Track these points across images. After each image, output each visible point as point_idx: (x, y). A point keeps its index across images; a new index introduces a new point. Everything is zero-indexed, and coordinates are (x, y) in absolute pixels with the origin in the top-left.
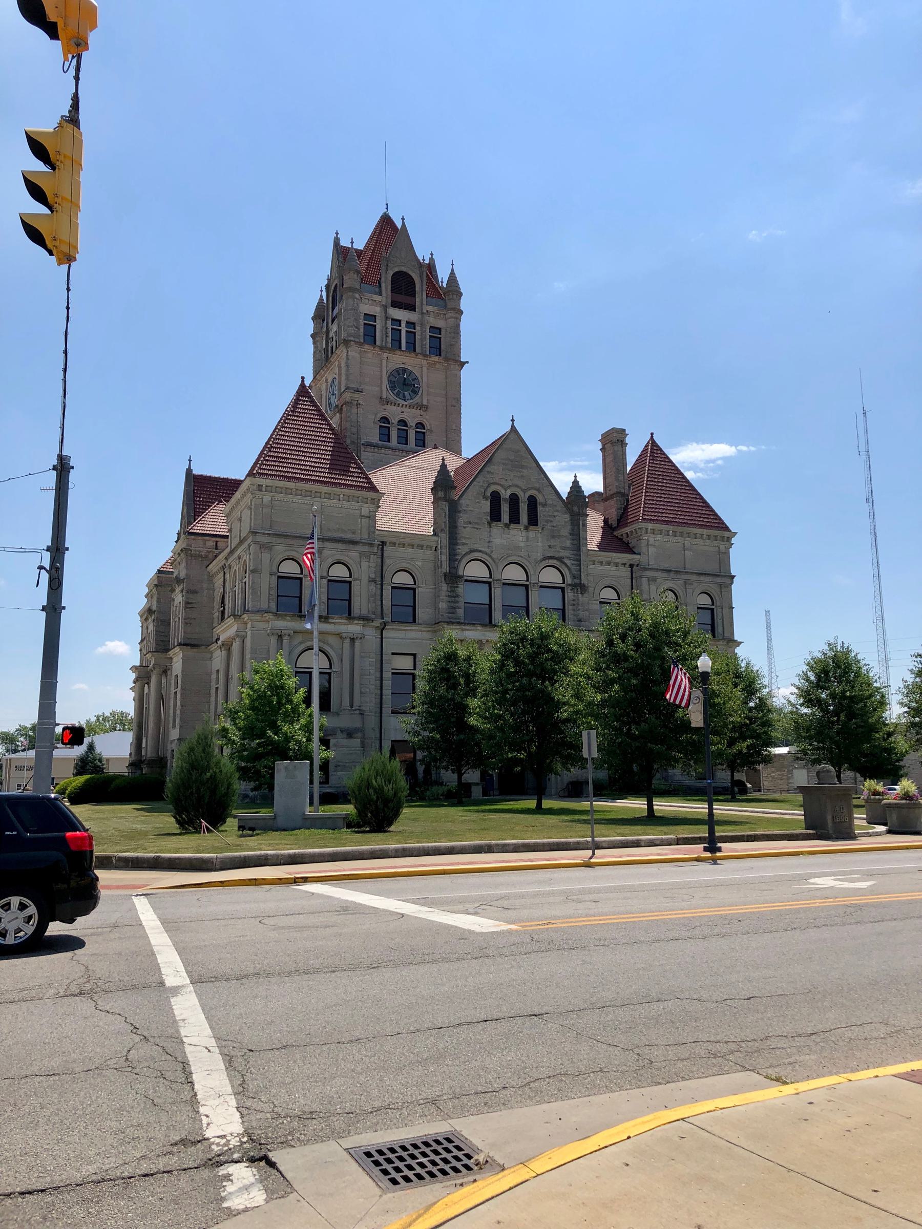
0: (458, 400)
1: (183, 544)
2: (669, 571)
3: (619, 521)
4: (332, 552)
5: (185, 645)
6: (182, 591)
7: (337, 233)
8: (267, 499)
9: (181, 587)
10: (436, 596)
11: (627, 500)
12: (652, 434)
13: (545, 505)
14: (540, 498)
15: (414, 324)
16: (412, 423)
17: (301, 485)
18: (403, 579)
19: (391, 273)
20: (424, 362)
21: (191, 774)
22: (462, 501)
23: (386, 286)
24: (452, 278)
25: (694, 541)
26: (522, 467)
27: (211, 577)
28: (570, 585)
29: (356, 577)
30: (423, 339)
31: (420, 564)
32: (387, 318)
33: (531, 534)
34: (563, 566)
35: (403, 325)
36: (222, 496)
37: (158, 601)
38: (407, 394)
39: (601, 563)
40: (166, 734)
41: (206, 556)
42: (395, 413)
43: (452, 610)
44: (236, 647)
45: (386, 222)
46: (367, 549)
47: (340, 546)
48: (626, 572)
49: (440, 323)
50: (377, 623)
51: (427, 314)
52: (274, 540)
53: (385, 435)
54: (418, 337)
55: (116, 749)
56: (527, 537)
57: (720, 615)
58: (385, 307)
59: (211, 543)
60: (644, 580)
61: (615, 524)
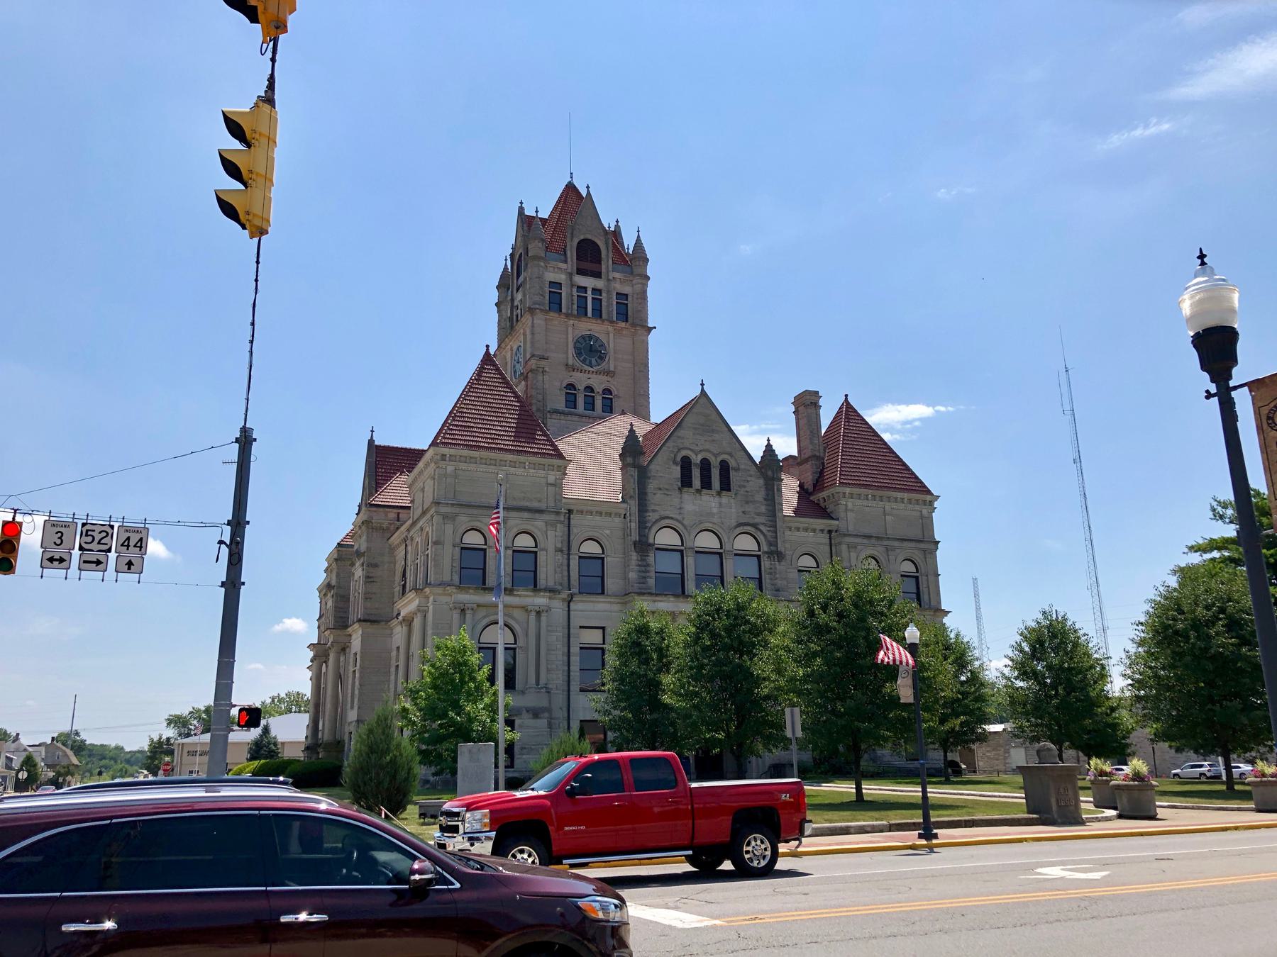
0: (647, 366)
1: (363, 516)
2: (869, 537)
3: (815, 486)
5: (365, 621)
8: (450, 469)
10: (626, 565)
13: (737, 470)
14: (732, 463)
17: (484, 454)
18: (591, 548)
19: (576, 241)
20: (611, 329)
22: (652, 467)
23: (572, 254)
25: (894, 505)
26: (713, 431)
27: (392, 550)
32: (572, 286)
33: (724, 500)
35: (589, 292)
37: (338, 575)
38: (593, 361)
39: (798, 529)
41: (388, 529)
42: (581, 380)
43: (643, 580)
44: (417, 622)
45: (570, 189)
46: (553, 517)
47: (526, 515)
48: (824, 538)
49: (626, 289)
50: (564, 595)
51: (614, 281)
52: (457, 510)
53: (571, 401)
58: (571, 275)
59: (392, 514)
60: (844, 547)
61: (811, 489)
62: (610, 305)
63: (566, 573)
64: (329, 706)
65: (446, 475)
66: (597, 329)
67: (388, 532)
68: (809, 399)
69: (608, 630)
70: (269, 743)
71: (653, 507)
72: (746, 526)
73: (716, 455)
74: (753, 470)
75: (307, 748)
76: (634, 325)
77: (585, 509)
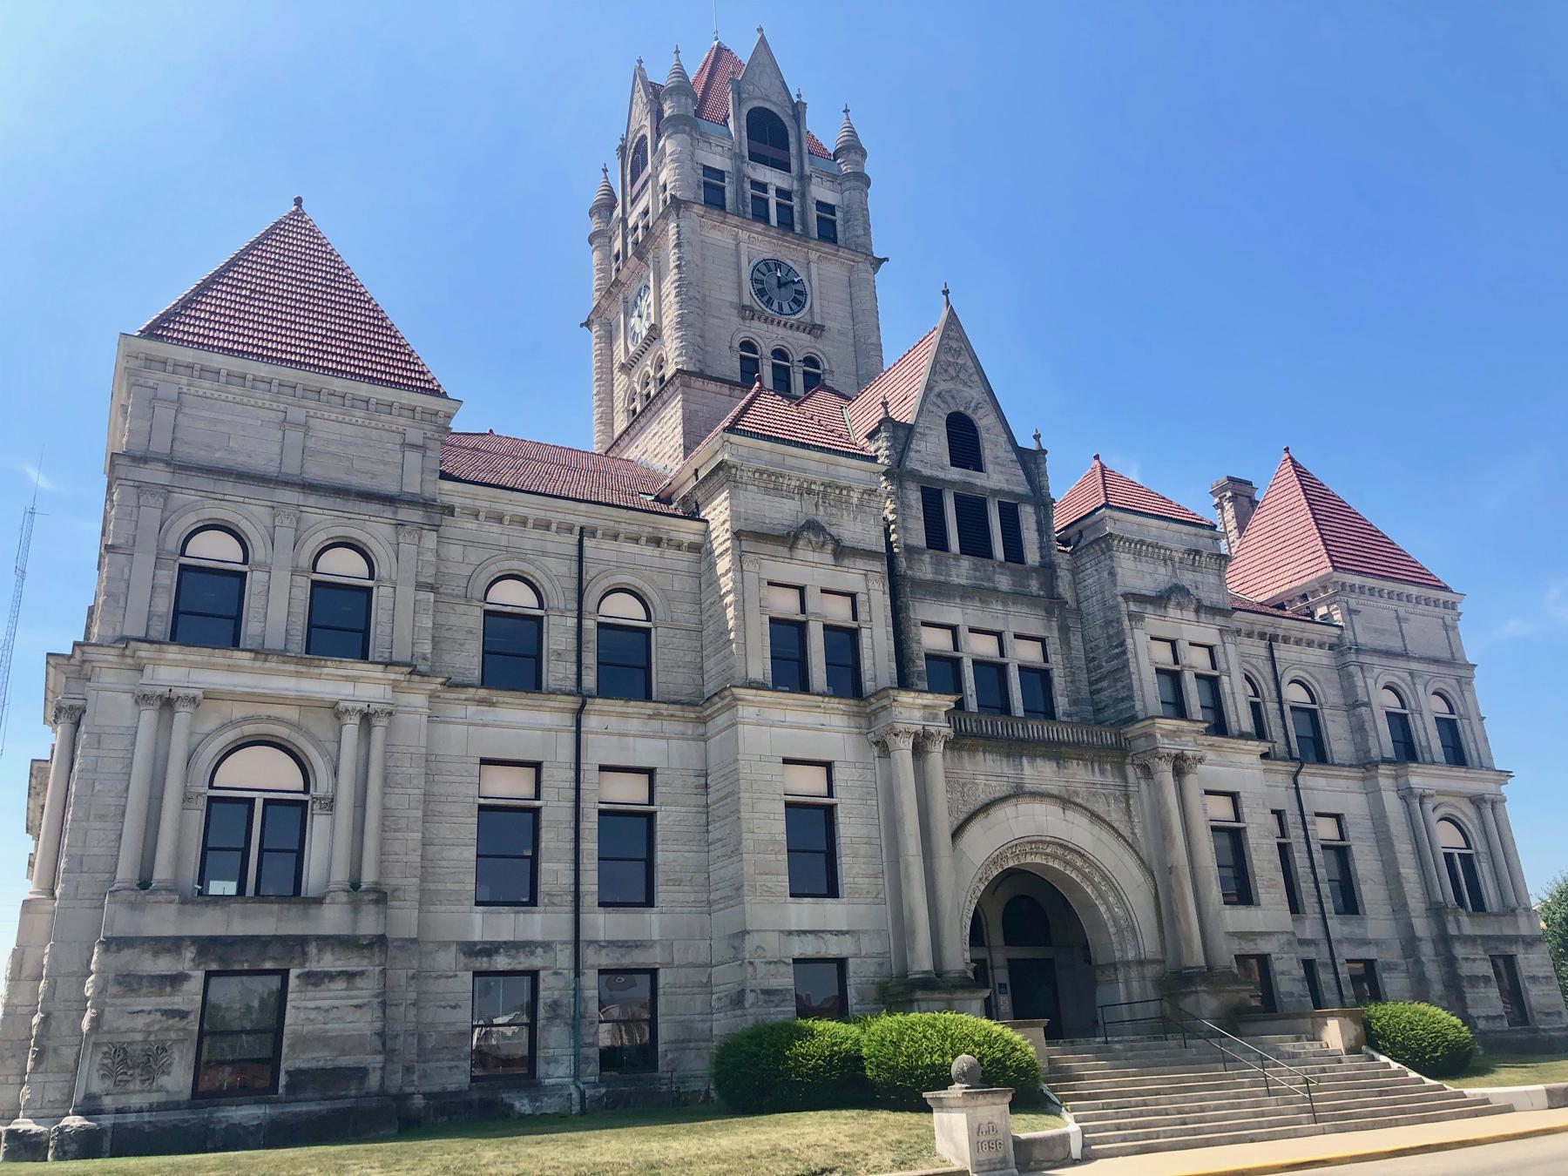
16: (797, 356)
18: (623, 609)
35: (772, 193)
42: (768, 337)
53: (749, 370)
57: (1419, 723)
66: (791, 254)
69: (658, 779)
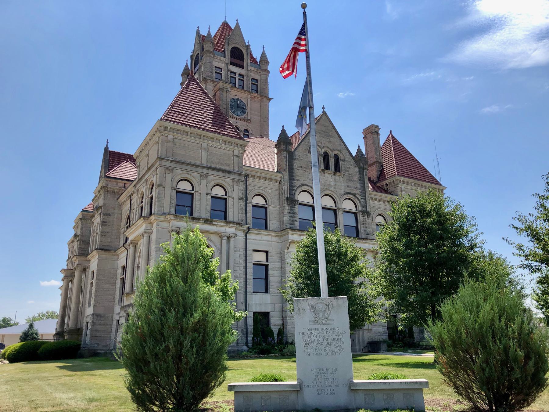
0: (268, 119)
1: (103, 184)
3: (379, 178)
4: (214, 177)
5: (100, 249)
6: (100, 214)
7: (198, 28)
8: (170, 137)
9: (100, 211)
10: (281, 213)
11: (382, 166)
12: (391, 131)
13: (344, 160)
14: (341, 156)
15: (257, 80)
17: (193, 130)
18: (259, 201)
19: (230, 47)
20: (249, 96)
21: (165, 315)
22: (296, 153)
23: (228, 53)
24: (263, 55)
26: (330, 136)
27: (120, 206)
28: (361, 211)
29: (230, 195)
30: (249, 84)
31: (270, 191)
32: (228, 70)
33: (337, 178)
34: (356, 199)
35: (237, 75)
36: (128, 158)
37: (82, 228)
38: (239, 113)
39: (376, 199)
40: (83, 310)
41: (118, 192)
43: (292, 222)
44: (143, 243)
45: (225, 25)
46: (237, 177)
47: (220, 174)
49: (257, 77)
50: (245, 228)
52: (175, 165)
54: (245, 83)
55: (47, 331)
56: (335, 180)
59: (121, 184)
61: (376, 180)
62: (248, 84)
63: (244, 215)
64: (73, 305)
65: (167, 141)
66: (242, 96)
67: (117, 194)
68: (374, 129)
69: (270, 254)
70: (33, 333)
71: (297, 178)
72: (350, 196)
73: (332, 151)
74: (352, 161)
75: (57, 334)
76: (261, 96)
77: (257, 174)
